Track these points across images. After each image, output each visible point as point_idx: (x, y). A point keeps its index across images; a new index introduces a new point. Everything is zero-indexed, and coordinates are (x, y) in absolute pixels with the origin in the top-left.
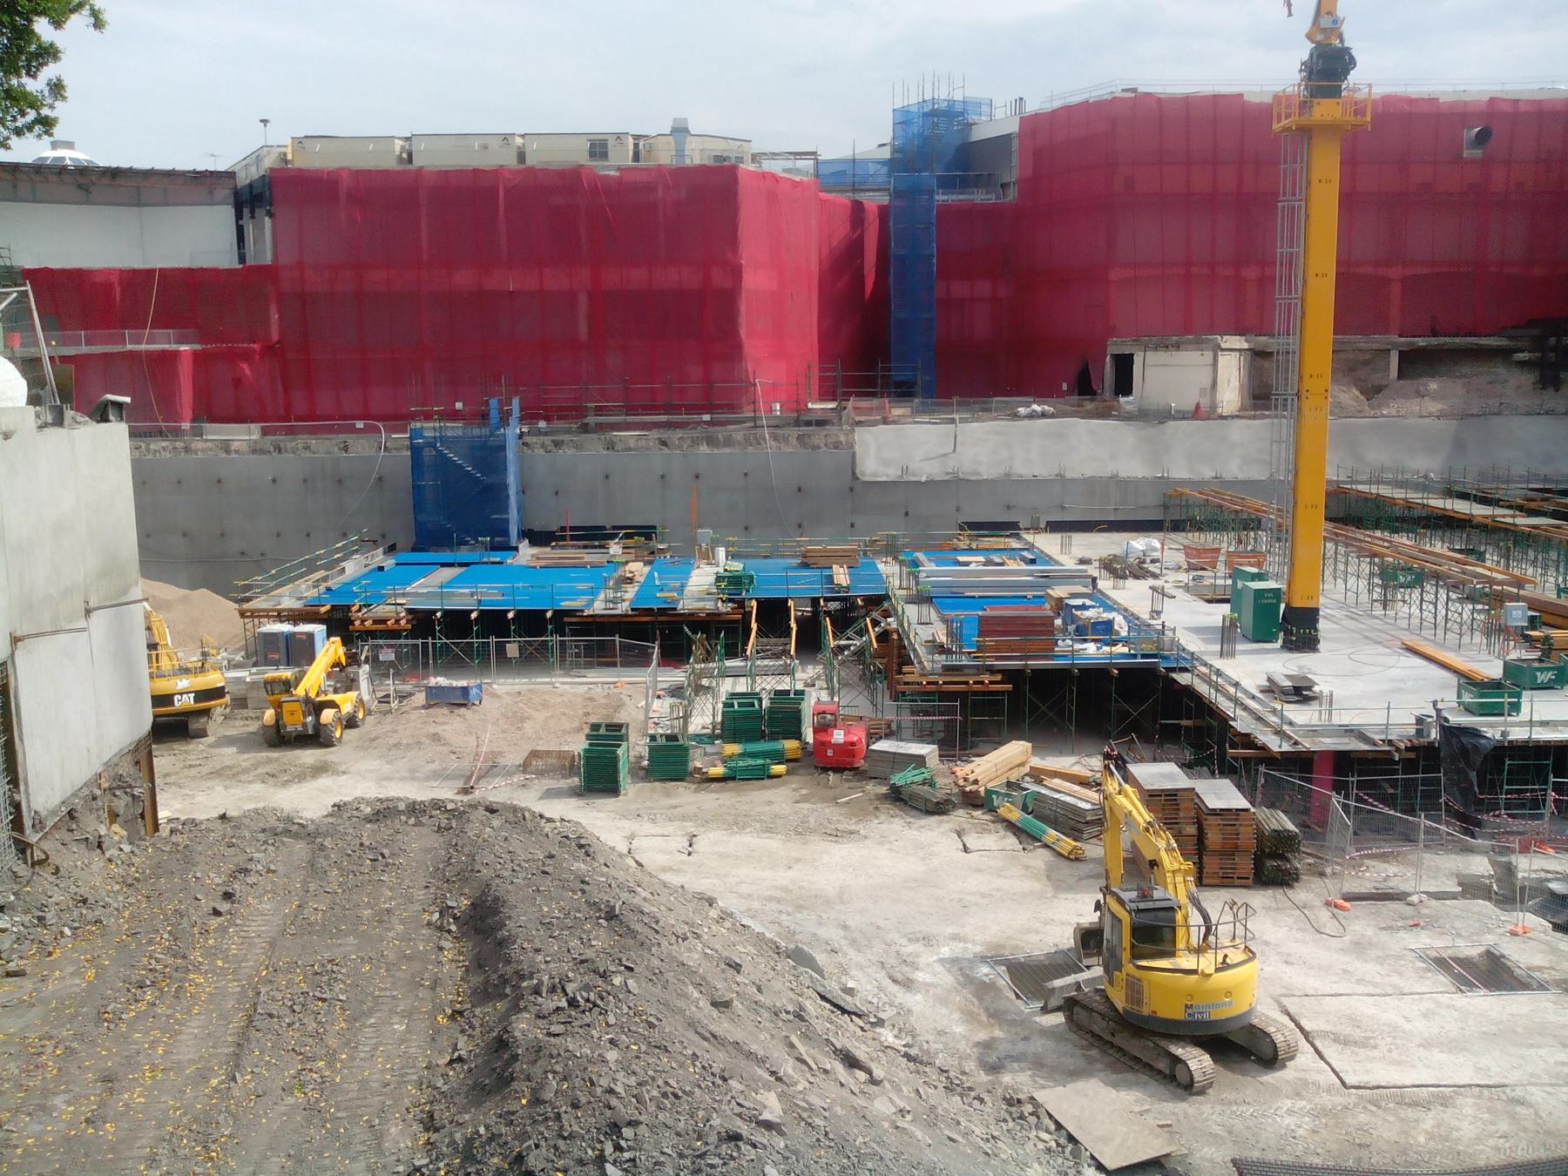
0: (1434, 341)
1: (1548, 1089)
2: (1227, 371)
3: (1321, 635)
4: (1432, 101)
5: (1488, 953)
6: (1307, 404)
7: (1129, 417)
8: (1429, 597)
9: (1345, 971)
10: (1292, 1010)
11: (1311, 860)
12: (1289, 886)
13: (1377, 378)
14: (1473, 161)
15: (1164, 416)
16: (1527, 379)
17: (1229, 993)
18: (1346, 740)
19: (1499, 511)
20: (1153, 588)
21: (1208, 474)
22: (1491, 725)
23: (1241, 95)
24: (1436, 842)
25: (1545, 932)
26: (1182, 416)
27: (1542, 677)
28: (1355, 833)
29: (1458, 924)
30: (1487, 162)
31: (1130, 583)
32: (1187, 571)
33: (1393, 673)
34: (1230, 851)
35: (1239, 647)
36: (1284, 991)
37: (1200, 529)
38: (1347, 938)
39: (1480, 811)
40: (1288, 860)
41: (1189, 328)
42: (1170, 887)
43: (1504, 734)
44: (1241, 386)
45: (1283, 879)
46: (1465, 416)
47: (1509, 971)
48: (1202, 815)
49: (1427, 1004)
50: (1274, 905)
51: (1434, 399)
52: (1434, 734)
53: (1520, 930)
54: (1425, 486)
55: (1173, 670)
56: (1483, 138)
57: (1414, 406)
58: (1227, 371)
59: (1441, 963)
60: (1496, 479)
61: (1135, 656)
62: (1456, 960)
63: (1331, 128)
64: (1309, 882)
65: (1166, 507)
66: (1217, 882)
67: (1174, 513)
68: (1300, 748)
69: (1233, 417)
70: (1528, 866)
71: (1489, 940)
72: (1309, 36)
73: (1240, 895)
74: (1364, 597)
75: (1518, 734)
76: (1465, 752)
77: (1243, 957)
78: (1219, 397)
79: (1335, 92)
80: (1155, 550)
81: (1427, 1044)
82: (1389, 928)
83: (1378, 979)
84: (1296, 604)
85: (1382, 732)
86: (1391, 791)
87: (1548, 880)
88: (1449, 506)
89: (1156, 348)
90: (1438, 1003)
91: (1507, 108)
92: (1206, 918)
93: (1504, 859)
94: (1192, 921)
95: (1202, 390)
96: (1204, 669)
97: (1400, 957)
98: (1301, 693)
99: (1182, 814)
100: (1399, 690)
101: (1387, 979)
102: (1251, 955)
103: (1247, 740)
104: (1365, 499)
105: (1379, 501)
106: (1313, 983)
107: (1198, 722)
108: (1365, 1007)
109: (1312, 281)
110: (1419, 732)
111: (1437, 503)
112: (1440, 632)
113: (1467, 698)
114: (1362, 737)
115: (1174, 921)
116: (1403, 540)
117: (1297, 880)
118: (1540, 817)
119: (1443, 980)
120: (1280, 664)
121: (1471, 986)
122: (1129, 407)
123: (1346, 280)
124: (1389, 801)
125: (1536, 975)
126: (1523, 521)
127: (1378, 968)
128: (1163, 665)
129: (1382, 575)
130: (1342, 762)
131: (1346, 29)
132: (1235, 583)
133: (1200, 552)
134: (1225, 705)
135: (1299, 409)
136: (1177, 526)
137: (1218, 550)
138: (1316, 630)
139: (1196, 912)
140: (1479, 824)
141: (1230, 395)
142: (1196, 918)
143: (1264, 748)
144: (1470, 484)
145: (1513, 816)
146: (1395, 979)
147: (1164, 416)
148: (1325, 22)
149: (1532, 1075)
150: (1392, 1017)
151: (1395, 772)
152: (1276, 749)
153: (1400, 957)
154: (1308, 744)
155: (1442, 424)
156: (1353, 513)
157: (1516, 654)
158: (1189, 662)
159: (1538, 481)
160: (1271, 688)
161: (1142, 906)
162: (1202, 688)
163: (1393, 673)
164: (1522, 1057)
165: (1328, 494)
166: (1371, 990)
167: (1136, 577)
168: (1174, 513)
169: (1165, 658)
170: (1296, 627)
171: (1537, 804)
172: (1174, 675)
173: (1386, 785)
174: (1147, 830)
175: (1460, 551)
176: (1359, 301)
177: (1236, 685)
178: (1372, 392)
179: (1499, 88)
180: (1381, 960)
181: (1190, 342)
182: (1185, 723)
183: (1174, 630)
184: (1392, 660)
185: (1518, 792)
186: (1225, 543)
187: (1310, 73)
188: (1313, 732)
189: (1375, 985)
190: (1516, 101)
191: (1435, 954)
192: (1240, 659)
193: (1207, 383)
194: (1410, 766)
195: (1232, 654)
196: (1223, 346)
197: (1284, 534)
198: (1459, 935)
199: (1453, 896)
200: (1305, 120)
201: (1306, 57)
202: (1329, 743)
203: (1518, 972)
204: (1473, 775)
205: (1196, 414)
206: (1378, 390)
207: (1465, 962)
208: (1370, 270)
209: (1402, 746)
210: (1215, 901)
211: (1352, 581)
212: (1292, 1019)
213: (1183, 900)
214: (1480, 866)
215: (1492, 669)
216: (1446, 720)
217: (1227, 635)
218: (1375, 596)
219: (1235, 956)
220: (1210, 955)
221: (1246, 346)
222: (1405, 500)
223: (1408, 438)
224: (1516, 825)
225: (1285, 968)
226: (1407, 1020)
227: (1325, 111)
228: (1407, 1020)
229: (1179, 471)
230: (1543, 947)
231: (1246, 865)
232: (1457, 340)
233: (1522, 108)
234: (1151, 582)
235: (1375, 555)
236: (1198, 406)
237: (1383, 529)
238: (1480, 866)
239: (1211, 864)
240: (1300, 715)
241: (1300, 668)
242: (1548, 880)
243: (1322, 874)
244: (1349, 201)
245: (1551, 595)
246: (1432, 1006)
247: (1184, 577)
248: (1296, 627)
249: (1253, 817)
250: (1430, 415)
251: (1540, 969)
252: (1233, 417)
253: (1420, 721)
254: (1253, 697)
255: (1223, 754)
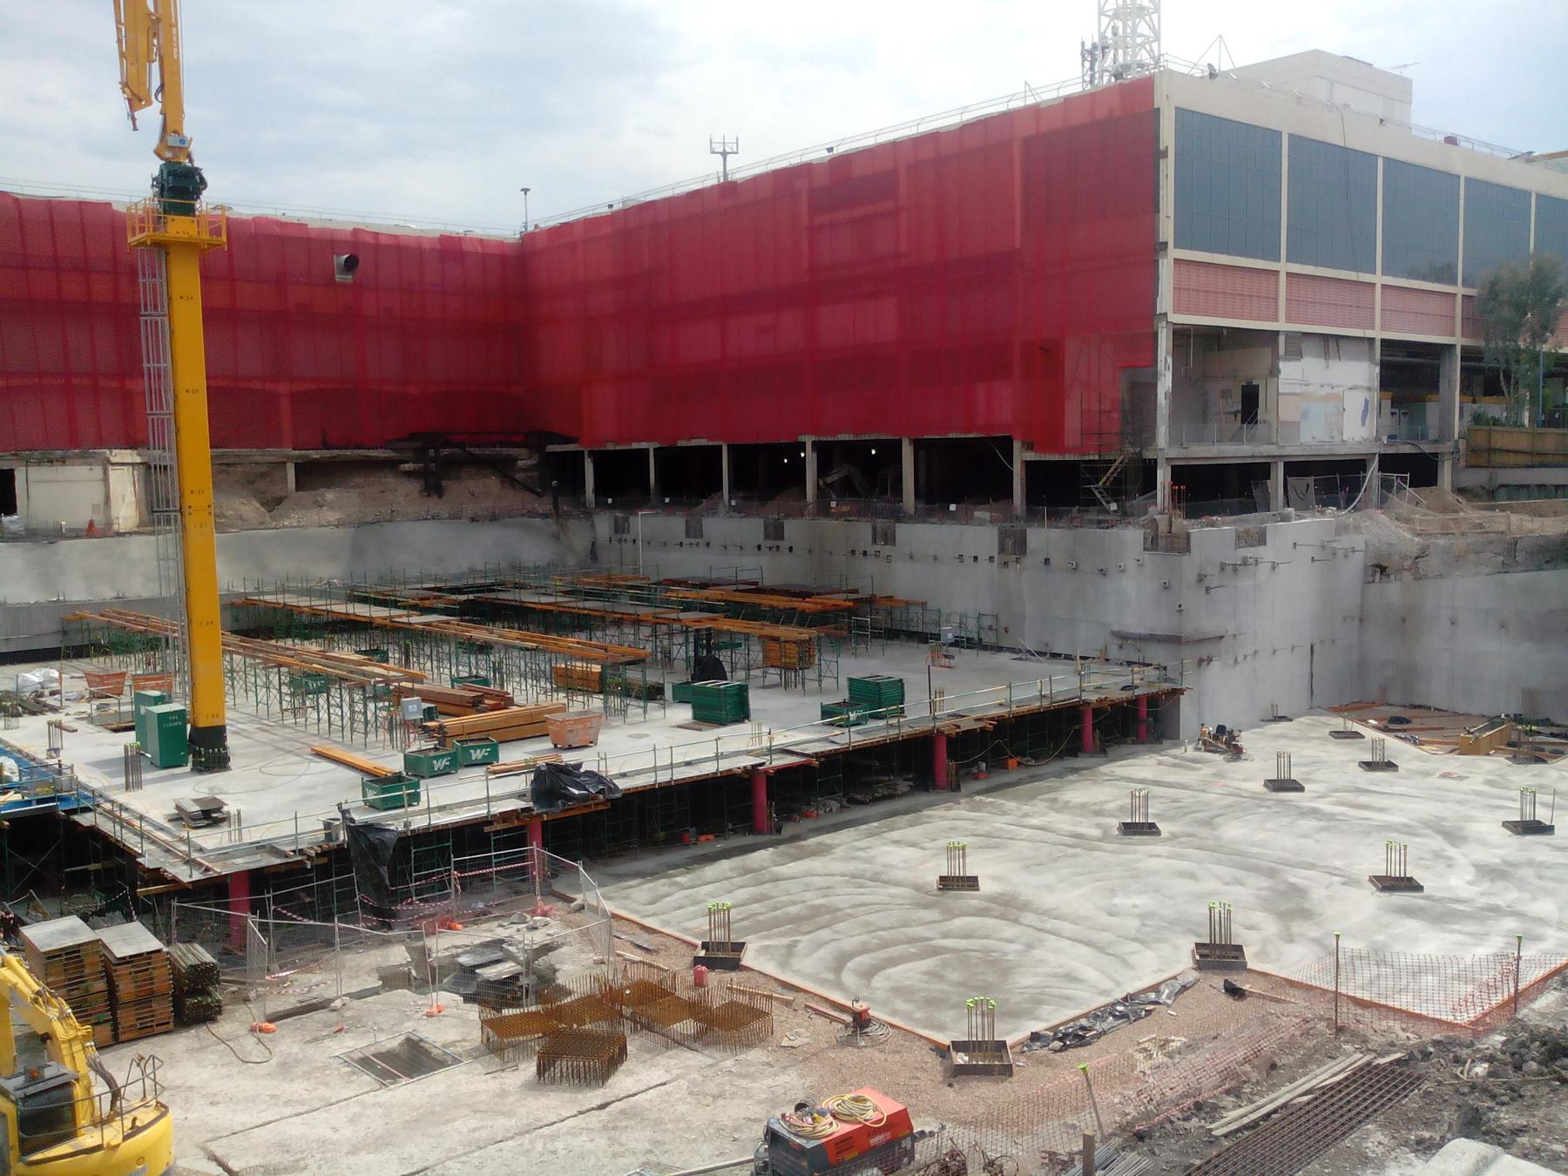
0: (327, 453)
1: (463, 1159)
2: (120, 486)
3: (231, 752)
4: (301, 226)
5: (408, 1040)
6: (191, 521)
7: (14, 538)
8: (335, 701)
9: (272, 1096)
10: (218, 1154)
11: (234, 988)
12: (213, 1020)
13: (276, 491)
14: (345, 286)
15: (54, 535)
16: (414, 487)
17: (140, 1159)
18: (259, 857)
19: (395, 612)
20: (50, 724)
21: (108, 594)
22: (396, 818)
23: (109, 204)
24: (354, 942)
25: (457, 1007)
26: (75, 534)
27: (438, 765)
28: (278, 950)
29: (379, 1019)
30: (357, 287)
31: (26, 720)
32: (89, 700)
33: (303, 781)
34: (144, 1000)
35: (146, 776)
36: (209, 1136)
37: (106, 654)
38: (273, 1062)
39: (395, 902)
40: (209, 994)
41: (73, 441)
42: (67, 1059)
43: (407, 825)
44: (138, 503)
45: (207, 1015)
46: (361, 524)
47: (427, 1053)
48: (110, 967)
49: (354, 1109)
50: (197, 1045)
51: (331, 509)
52: (343, 836)
53: (435, 1010)
54: (328, 593)
55: (74, 811)
56: (351, 264)
57: (314, 516)
58: (120, 486)
59: (365, 1063)
60: (394, 581)
61: (29, 803)
62: (379, 1056)
63: (189, 246)
64: (232, 1011)
65: (65, 633)
66: (135, 1035)
67: (72, 639)
68: (211, 874)
69: (130, 534)
70: (443, 945)
71: (408, 1027)
72: (157, 153)
73: (144, 1048)
74: (275, 707)
75: (419, 822)
76: (374, 850)
77: (153, 1115)
78: (114, 513)
79: (189, 211)
80: (52, 680)
81: (354, 1151)
82: (315, 1040)
83: (306, 1095)
84: (202, 723)
85: (292, 843)
86: (308, 900)
87: (458, 955)
88: (351, 611)
89: (39, 463)
90: (363, 1105)
91: (369, 239)
92: (110, 1081)
93: (420, 944)
94: (95, 1091)
95: (95, 507)
96: (108, 806)
97: (325, 1068)
98: (210, 816)
99: (87, 971)
100: (308, 798)
101: (314, 1094)
102: (163, 1110)
103: (157, 876)
104: (275, 609)
105: (289, 611)
106: (241, 1118)
107: (107, 864)
108: (295, 1129)
109: (182, 395)
110: (328, 836)
111: (340, 608)
112: (347, 733)
113: (371, 796)
114: (274, 851)
115: (70, 1097)
116: (313, 647)
117: (220, 1012)
118: (448, 896)
119: (368, 1079)
120: (189, 788)
121: (394, 1078)
122: (13, 528)
123: (222, 395)
124: (306, 911)
125: (451, 1050)
126: (417, 619)
127: (305, 1084)
128: (62, 808)
129: (291, 683)
130: (257, 880)
131: (194, 149)
132: (138, 709)
133: (102, 679)
134: (131, 841)
135: (184, 527)
136: (79, 652)
137: (123, 675)
138: (225, 748)
139: (100, 1079)
140: (393, 915)
141: (126, 511)
142: (100, 1087)
143: (175, 880)
144: (371, 586)
145: (425, 901)
146: (323, 1091)
147: (54, 535)
148: (172, 140)
149: (450, 1150)
150: (322, 1131)
151: (310, 880)
152: (186, 879)
153: (325, 1068)
154: (219, 869)
155: (341, 531)
156: (257, 624)
157: (418, 744)
158: (91, 801)
159: (430, 581)
160: (181, 817)
161: (31, 1090)
162: (107, 827)
163: (303, 781)
164: (441, 1135)
165: (224, 607)
166: (299, 1109)
167: (34, 713)
168: (72, 639)
169: (61, 799)
170: (203, 747)
171: (443, 885)
172: (76, 818)
173: (302, 895)
174: (36, 1001)
175: (365, 653)
176: (237, 413)
177: (141, 818)
178: (273, 503)
179: (359, 220)
180: (306, 1076)
181: (76, 456)
182: (92, 867)
183: (71, 768)
184: (301, 768)
185: (427, 877)
186: (132, 665)
187: (162, 188)
188: (224, 854)
189: (302, 1103)
190: (376, 234)
191: (358, 1055)
192: (148, 789)
193: (99, 498)
194: (323, 871)
195: (138, 785)
196: (113, 460)
197: (188, 650)
198: (380, 1030)
199: (374, 992)
200: (159, 236)
201: (156, 173)
202: (241, 864)
203: (435, 1051)
204: (384, 870)
205: (90, 531)
206: (279, 501)
207: (387, 1056)
208: (258, 386)
209: (313, 853)
210: (120, 1063)
211: (262, 692)
212: (221, 1164)
213: (83, 1068)
214: (398, 955)
215: (394, 763)
216: (352, 820)
217: (131, 766)
218: (285, 705)
219: (144, 1116)
220: (117, 1124)
221: (138, 460)
222: (310, 607)
223: (307, 547)
224: (428, 908)
225: (214, 1111)
226: (335, 1129)
227: (179, 227)
228: (335, 1129)
229: (76, 592)
230: (455, 1021)
231: (163, 1009)
232: (348, 453)
233: (383, 241)
234: (51, 717)
235: (280, 665)
236: (91, 524)
237: (294, 637)
238: (398, 955)
239: (127, 1017)
240: (209, 839)
241: (211, 789)
242: (458, 955)
243: (246, 1000)
244: (213, 317)
245: (446, 686)
246: (358, 1109)
247: (86, 707)
248: (203, 747)
249: (170, 959)
250: (329, 524)
251: (453, 1043)
252: (130, 534)
253: (327, 825)
254: (162, 829)
255: (135, 897)
